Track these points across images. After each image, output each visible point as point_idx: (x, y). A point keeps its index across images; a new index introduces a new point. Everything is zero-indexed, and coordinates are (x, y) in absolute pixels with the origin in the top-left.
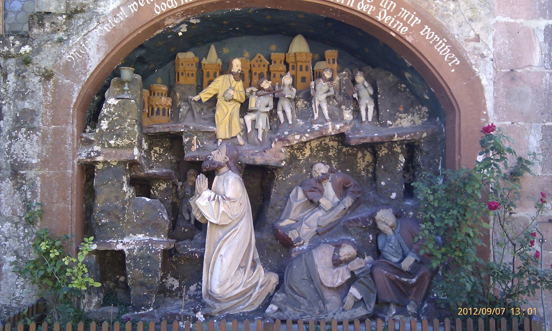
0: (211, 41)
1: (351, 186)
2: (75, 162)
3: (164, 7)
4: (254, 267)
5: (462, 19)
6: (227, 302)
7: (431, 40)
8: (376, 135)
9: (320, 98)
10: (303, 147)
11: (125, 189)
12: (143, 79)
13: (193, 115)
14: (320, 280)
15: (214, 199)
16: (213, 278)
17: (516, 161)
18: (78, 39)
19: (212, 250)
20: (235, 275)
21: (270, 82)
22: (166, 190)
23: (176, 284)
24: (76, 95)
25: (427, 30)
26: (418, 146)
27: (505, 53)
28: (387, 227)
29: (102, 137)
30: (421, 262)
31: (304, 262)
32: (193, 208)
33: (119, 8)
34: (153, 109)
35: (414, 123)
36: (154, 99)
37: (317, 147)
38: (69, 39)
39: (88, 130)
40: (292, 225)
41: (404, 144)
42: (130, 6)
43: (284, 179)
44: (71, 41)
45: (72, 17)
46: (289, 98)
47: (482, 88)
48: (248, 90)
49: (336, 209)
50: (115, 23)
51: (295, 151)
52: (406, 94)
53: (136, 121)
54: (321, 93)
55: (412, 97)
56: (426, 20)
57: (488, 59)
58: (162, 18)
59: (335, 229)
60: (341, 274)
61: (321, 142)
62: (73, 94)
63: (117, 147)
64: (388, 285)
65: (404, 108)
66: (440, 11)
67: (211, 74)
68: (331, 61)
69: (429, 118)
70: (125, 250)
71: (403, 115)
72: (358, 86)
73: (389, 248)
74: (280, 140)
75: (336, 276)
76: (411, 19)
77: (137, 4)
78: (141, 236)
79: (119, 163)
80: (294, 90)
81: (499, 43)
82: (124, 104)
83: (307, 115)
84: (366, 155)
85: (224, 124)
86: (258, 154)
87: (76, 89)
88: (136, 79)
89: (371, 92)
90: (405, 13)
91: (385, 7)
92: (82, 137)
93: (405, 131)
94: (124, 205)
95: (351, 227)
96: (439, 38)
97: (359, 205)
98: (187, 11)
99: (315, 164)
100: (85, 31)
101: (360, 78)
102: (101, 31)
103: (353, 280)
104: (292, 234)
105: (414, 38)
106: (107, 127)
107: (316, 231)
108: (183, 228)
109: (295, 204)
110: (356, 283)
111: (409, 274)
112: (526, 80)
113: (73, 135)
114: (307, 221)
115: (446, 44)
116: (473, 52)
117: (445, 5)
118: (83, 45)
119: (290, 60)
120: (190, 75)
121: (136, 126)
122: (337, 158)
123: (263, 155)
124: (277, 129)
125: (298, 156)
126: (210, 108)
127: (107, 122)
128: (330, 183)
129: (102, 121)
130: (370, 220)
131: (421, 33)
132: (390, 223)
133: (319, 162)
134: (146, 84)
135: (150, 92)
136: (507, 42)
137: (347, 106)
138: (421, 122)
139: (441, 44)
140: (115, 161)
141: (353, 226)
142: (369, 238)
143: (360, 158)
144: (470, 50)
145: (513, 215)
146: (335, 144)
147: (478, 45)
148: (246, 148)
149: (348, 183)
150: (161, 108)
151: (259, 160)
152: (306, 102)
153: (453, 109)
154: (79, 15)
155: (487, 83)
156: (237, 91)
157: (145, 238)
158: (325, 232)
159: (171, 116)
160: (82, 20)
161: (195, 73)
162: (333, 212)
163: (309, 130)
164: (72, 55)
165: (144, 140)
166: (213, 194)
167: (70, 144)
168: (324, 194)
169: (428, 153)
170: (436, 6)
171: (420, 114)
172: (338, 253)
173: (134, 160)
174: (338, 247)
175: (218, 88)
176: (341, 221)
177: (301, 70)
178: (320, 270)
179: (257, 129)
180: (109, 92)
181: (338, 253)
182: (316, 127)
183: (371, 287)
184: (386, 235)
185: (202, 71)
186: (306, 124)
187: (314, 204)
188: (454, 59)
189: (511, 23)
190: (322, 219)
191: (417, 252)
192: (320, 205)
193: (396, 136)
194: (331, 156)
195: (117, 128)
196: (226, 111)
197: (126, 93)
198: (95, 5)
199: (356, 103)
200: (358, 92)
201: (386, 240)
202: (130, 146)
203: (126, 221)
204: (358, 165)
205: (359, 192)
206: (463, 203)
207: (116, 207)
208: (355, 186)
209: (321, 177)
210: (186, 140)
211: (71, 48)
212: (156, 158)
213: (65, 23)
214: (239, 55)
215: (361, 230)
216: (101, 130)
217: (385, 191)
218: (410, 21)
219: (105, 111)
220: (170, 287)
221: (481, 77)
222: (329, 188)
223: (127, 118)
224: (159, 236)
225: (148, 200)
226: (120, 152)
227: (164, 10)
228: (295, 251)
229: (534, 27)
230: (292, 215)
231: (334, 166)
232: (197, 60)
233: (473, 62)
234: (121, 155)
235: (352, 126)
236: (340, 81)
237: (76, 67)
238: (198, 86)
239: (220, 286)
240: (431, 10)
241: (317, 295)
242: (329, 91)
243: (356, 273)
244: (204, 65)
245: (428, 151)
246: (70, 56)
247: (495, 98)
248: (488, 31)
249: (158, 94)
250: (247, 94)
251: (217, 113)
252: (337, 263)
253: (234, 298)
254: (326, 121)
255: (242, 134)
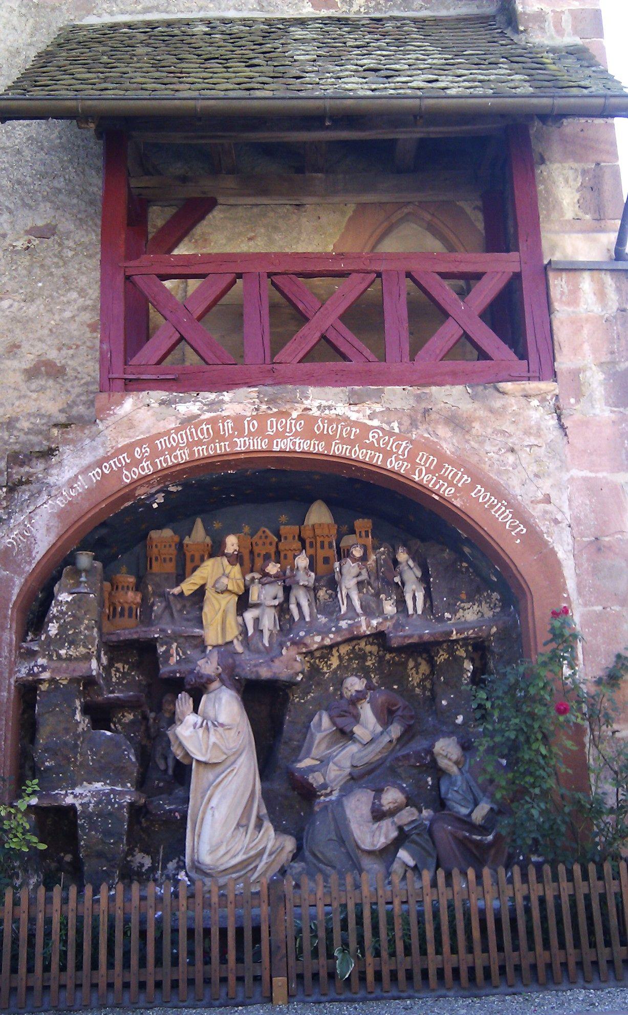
0: (196, 514)
1: (398, 709)
2: (12, 681)
3: (135, 473)
4: (259, 826)
5: (524, 476)
6: (223, 876)
7: (485, 503)
8: (427, 631)
9: (349, 584)
10: (328, 654)
11: (78, 717)
12: (104, 567)
13: (172, 615)
14: (355, 841)
15: (201, 726)
16: (201, 843)
17: (614, 659)
18: (22, 518)
19: (199, 800)
20: (233, 836)
21: (279, 565)
22: (132, 722)
23: (147, 862)
24: (16, 591)
25: (480, 491)
26: (489, 647)
27: (586, 516)
28: (450, 763)
29: (49, 646)
30: (500, 812)
31: (330, 815)
32: (172, 743)
33: (76, 476)
34: (115, 609)
35: (483, 616)
36: (117, 594)
37: (348, 654)
38: (10, 518)
39: (29, 638)
40: (315, 766)
41: (469, 644)
42: (91, 474)
43: (302, 701)
44: (12, 521)
45: (15, 491)
46: (305, 586)
47: (558, 563)
48: (248, 577)
49: (377, 742)
50: (71, 496)
51: (317, 661)
52: (469, 576)
53: (96, 622)
54: (348, 577)
55: (478, 579)
56: (478, 478)
57: (564, 525)
58: (132, 487)
59: (378, 772)
60: (384, 830)
61: (354, 648)
62: (13, 589)
63: (69, 659)
64: (454, 846)
65: (467, 594)
66: (496, 466)
67: (197, 557)
68: (363, 534)
69: (502, 607)
70: (77, 805)
71: (467, 605)
72: (401, 567)
73: (454, 793)
74: (294, 643)
75: (377, 833)
76: (458, 478)
77: (100, 471)
78: (98, 785)
79: (71, 681)
80: (313, 574)
81: (577, 504)
82: (80, 600)
83: (332, 609)
84: (420, 664)
85: (215, 624)
86: (262, 665)
87: (17, 582)
88: (95, 567)
89: (419, 574)
90: (449, 470)
91: (422, 464)
92: (21, 647)
93: (467, 625)
94: (76, 740)
95: (400, 767)
96: (496, 501)
97: (413, 737)
98: (166, 476)
99: (345, 678)
100: (32, 508)
101: (402, 556)
102: (52, 507)
103: (402, 838)
104: (313, 778)
105: (463, 501)
106: (57, 632)
107: (350, 774)
108: (156, 782)
109: (319, 736)
110: (407, 843)
111: (483, 829)
112: (617, 550)
113: (10, 644)
114: (336, 759)
115: (506, 508)
116: (543, 516)
117: (502, 458)
118: (28, 525)
119: (307, 534)
120: (168, 560)
121: (96, 630)
122: (379, 669)
123: (270, 666)
124: (290, 631)
125: (321, 667)
126: (194, 604)
127: (56, 625)
128: (369, 705)
129: (50, 625)
130: (426, 755)
131: (473, 494)
132: (454, 757)
133: (352, 675)
134: (108, 576)
135: (112, 585)
136: (588, 502)
137: (389, 595)
138: (491, 613)
139: (500, 508)
140: (66, 679)
141: (403, 766)
142: (427, 782)
143: (411, 669)
144: (538, 514)
145: (617, 735)
146: (374, 649)
147: (548, 507)
148: (246, 656)
149: (396, 705)
150: (126, 606)
151: (265, 673)
152: (329, 592)
153: (524, 594)
154: (24, 487)
155: (565, 556)
156: (232, 579)
157: (104, 788)
158: (362, 776)
159: (140, 618)
160: (28, 494)
161: (174, 557)
162: (374, 745)
163: (333, 629)
164: (13, 538)
165: (103, 652)
166: (200, 720)
167: (6, 657)
168: (361, 722)
169: (501, 656)
170: (490, 459)
171: (490, 603)
172: (380, 799)
173: (92, 676)
174: (379, 792)
175: (205, 575)
176: (386, 760)
177: (322, 547)
178: (354, 826)
179: (262, 631)
180: (60, 585)
181: (380, 801)
182: (343, 624)
183: (427, 848)
184: (450, 775)
185: (184, 554)
186: (331, 621)
187: (344, 735)
188: (518, 526)
189: (590, 478)
190: (358, 756)
191: (492, 797)
192: (355, 735)
193: (454, 633)
194: (369, 666)
195: (70, 632)
196: (217, 607)
197: (83, 585)
198: (45, 474)
199: (399, 589)
200: (401, 574)
201: (451, 783)
202: (87, 657)
203: (78, 763)
204: (410, 679)
205: (412, 717)
206: (529, 709)
207: (65, 743)
208: (405, 708)
209: (355, 696)
210: (161, 650)
211: (12, 530)
212: (118, 679)
213: (5, 498)
214: (235, 531)
215: (415, 771)
216: (48, 637)
217: (448, 714)
218: (456, 479)
219: (54, 610)
220: (138, 867)
221: (556, 549)
222: (366, 711)
223: (83, 619)
224: (124, 785)
225: (108, 733)
226: (72, 665)
227: (135, 477)
228: (319, 803)
229: (622, 482)
230: (314, 752)
231: (374, 681)
232: (177, 539)
233: (544, 529)
234: (74, 670)
235: (394, 621)
236: (377, 561)
237: (18, 553)
238: (178, 575)
239: (212, 852)
240: (483, 465)
241: (351, 863)
242: (359, 575)
243: (406, 829)
244: (187, 546)
245: (501, 653)
246: (11, 540)
247: (577, 575)
248: (561, 489)
249: (123, 587)
250: (247, 583)
251: (206, 609)
252: (378, 815)
253: (230, 871)
254: (358, 615)
255: (240, 638)
